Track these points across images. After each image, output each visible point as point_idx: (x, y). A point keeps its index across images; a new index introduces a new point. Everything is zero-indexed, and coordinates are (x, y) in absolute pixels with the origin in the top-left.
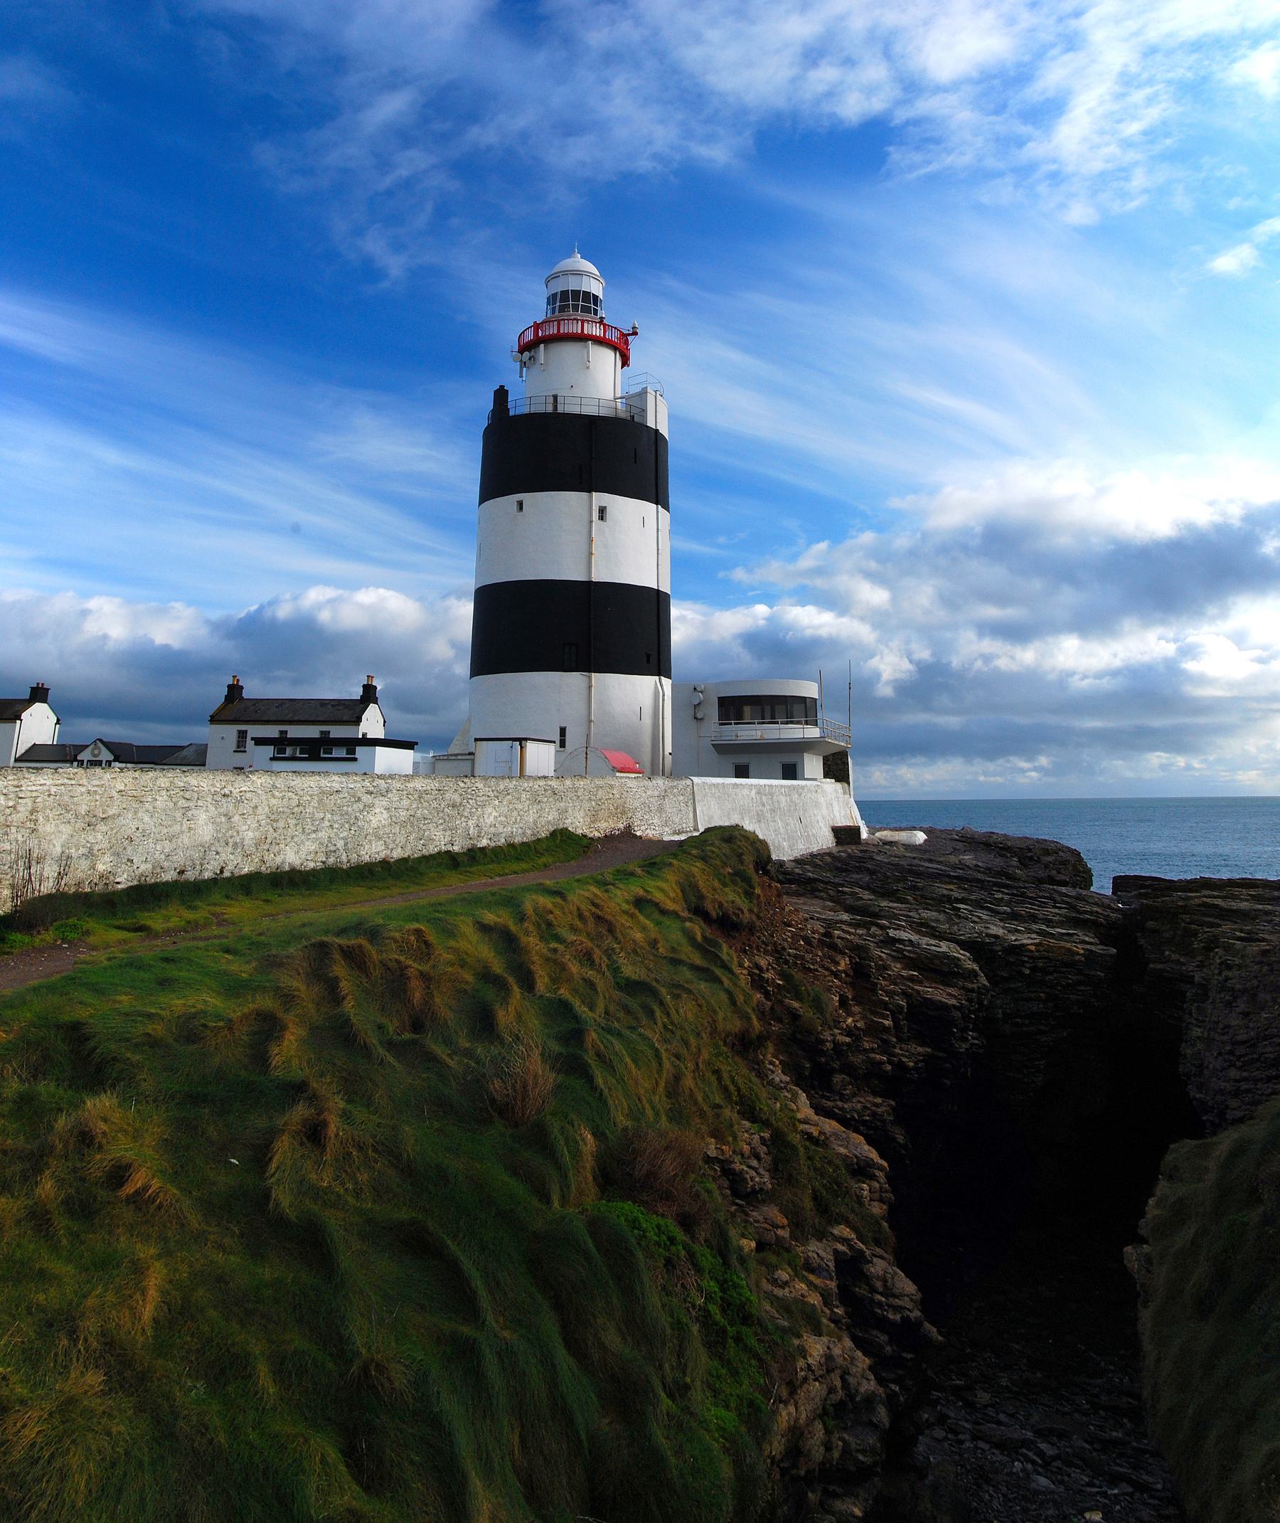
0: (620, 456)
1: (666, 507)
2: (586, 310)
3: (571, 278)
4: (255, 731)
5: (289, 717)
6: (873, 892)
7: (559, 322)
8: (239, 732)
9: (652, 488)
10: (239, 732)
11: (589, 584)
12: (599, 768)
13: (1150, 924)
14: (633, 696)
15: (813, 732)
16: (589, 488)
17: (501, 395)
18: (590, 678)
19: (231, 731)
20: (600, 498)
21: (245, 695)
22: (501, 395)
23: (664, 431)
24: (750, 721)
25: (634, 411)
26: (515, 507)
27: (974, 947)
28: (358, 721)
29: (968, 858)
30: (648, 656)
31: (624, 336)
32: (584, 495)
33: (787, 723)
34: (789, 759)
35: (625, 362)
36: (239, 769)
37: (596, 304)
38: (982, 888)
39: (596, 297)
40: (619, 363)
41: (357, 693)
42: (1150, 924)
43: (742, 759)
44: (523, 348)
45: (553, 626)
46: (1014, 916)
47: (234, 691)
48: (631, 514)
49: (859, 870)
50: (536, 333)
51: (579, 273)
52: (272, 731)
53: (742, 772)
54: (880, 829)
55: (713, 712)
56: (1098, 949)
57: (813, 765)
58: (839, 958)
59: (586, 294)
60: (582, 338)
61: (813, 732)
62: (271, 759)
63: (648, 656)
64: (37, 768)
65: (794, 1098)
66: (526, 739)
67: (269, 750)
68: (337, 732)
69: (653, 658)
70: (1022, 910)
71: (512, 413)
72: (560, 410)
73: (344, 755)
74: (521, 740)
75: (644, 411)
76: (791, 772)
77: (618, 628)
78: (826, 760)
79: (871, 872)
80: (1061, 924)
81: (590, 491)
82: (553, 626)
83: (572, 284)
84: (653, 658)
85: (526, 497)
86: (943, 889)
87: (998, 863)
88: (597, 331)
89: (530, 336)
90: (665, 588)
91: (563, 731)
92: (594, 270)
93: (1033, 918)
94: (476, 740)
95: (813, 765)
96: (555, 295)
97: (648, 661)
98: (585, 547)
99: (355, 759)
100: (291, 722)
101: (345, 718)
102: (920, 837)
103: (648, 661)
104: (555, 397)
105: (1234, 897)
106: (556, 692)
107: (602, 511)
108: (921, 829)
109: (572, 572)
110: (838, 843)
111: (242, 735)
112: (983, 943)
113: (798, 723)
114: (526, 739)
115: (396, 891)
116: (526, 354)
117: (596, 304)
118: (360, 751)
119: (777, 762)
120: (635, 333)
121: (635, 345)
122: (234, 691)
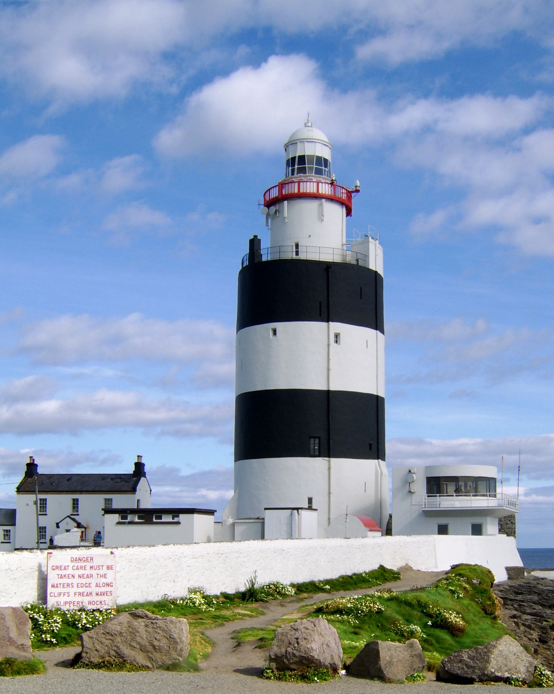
0: (345, 294)
1: (382, 332)
2: (319, 172)
5: (79, 488)
7: (299, 183)
8: (74, 500)
10: (74, 500)
14: (353, 476)
17: (254, 243)
18: (329, 461)
19: (30, 498)
20: (336, 327)
21: (40, 471)
22: (254, 243)
23: (381, 271)
25: (359, 256)
26: (271, 333)
30: (370, 445)
31: (349, 193)
32: (325, 324)
34: (477, 520)
35: (349, 213)
37: (326, 166)
39: (326, 161)
40: (345, 215)
41: (130, 469)
43: (443, 521)
44: (269, 204)
47: (31, 467)
48: (355, 336)
50: (280, 191)
53: (443, 530)
54: (533, 570)
59: (319, 159)
60: (316, 197)
62: (119, 523)
63: (370, 445)
66: (301, 508)
67: (116, 517)
69: (374, 448)
71: (264, 259)
72: (302, 256)
73: (171, 520)
74: (297, 509)
76: (477, 530)
77: (344, 425)
78: (500, 520)
79: (539, 594)
81: (328, 321)
84: (374, 448)
85: (279, 326)
88: (325, 189)
89: (275, 193)
90: (381, 394)
91: (310, 500)
94: (266, 509)
96: (293, 159)
97: (370, 449)
99: (178, 523)
100: (81, 492)
103: (370, 449)
104: (297, 246)
106: (300, 474)
107: (337, 336)
109: (314, 382)
110: (509, 578)
113: (483, 495)
116: (273, 209)
118: (182, 517)
120: (357, 191)
121: (356, 200)
122: (31, 467)
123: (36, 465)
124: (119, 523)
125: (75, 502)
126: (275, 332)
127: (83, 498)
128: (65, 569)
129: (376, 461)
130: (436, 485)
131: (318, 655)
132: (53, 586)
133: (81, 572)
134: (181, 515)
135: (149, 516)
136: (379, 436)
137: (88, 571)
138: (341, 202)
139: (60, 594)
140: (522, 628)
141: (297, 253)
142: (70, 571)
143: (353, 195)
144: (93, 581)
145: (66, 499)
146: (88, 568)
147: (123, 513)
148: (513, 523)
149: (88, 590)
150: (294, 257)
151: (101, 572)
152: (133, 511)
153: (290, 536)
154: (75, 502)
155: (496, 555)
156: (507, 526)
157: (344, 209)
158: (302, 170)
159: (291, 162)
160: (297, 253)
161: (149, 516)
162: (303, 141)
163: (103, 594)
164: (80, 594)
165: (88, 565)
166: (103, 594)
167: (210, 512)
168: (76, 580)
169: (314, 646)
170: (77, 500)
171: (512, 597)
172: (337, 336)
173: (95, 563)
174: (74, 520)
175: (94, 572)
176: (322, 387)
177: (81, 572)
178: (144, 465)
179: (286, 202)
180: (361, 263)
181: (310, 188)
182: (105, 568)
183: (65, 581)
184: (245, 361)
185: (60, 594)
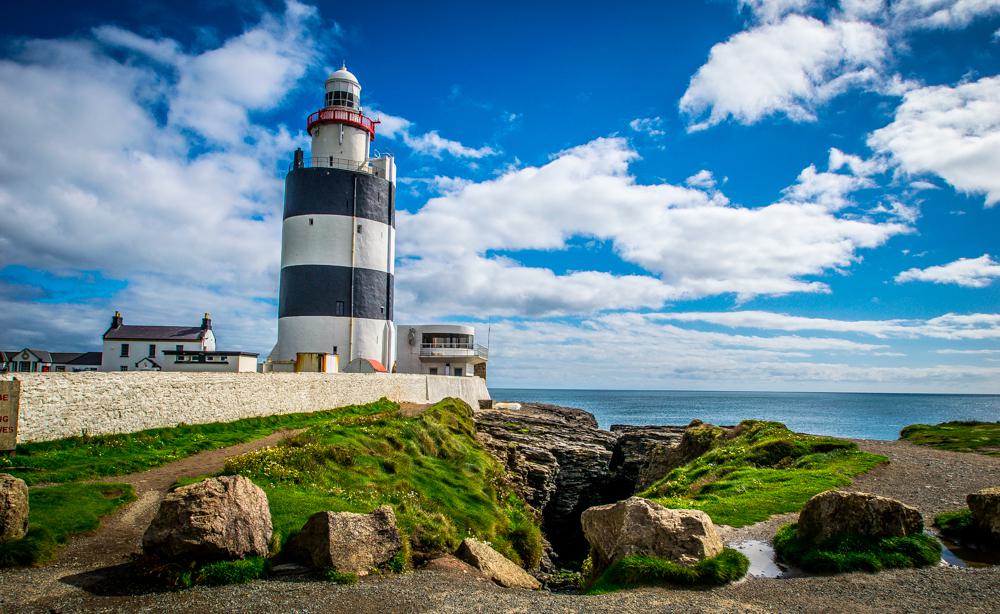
3: (342, 84)
4: (161, 346)
12: (361, 373)
13: (628, 442)
15: (471, 353)
19: (118, 345)
21: (124, 323)
24: (433, 348)
27: (554, 451)
28: (200, 339)
34: (458, 366)
36: (124, 368)
41: (199, 324)
42: (628, 442)
43: (434, 366)
45: (317, 291)
46: (571, 439)
49: (498, 419)
51: (347, 82)
52: (172, 346)
53: (433, 371)
55: (419, 338)
56: (605, 452)
57: (469, 369)
60: (348, 123)
61: (471, 353)
62: (176, 362)
64: (92, 369)
65: (641, 515)
67: (174, 358)
68: (188, 347)
70: (574, 436)
76: (459, 372)
80: (590, 442)
82: (317, 291)
83: (342, 88)
86: (539, 428)
89: (316, 118)
92: (355, 80)
93: (579, 440)
95: (469, 369)
96: (331, 93)
100: (157, 340)
104: (331, 158)
105: (664, 431)
107: (359, 227)
111: (153, 348)
114: (238, 354)
115: (832, 420)
118: (229, 359)
122: (116, 321)
124: (176, 362)
126: (312, 222)
130: (428, 339)
131: (224, 542)
135: (202, 357)
136: (390, 309)
141: (331, 165)
143: (376, 125)
145: (146, 345)
148: (484, 369)
153: (320, 371)
155: (472, 391)
156: (480, 370)
158: (337, 103)
159: (329, 96)
160: (331, 165)
161: (202, 357)
167: (255, 356)
169: (219, 524)
171: (485, 422)
172: (359, 227)
174: (151, 361)
184: (289, 243)
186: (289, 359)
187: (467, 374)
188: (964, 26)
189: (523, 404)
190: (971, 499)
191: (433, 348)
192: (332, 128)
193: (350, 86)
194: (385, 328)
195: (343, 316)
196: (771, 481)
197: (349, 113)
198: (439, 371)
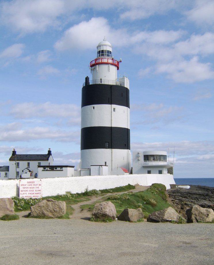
0: (117, 95)
1: (129, 108)
2: (108, 55)
6: (182, 197)
8: (28, 163)
9: (126, 103)
10: (28, 163)
11: (111, 127)
14: (120, 155)
16: (111, 103)
17: (87, 79)
18: (112, 150)
20: (114, 106)
21: (17, 153)
22: (87, 79)
23: (128, 88)
24: (150, 161)
25: (121, 83)
26: (93, 108)
28: (48, 160)
29: (200, 192)
31: (118, 63)
33: (160, 161)
34: (160, 169)
35: (118, 69)
37: (110, 54)
38: (203, 196)
39: (110, 52)
41: (47, 153)
43: (149, 169)
45: (94, 138)
47: (14, 153)
48: (120, 109)
50: (95, 62)
53: (149, 172)
55: (142, 158)
57: (165, 171)
58: (178, 205)
60: (107, 64)
62: (43, 170)
66: (103, 165)
67: (42, 169)
69: (126, 145)
71: (90, 84)
73: (60, 169)
75: (124, 83)
76: (160, 172)
77: (118, 138)
78: (168, 169)
82: (94, 138)
85: (95, 106)
86: (195, 196)
87: (206, 193)
88: (110, 61)
89: (94, 62)
91: (106, 163)
94: (91, 166)
95: (165, 171)
96: (100, 51)
98: (111, 118)
99: (62, 170)
100: (30, 160)
101: (45, 159)
102: (188, 187)
103: (125, 146)
104: (101, 80)
107: (114, 109)
108: (188, 185)
110: (171, 188)
112: (203, 205)
116: (93, 68)
117: (110, 54)
118: (64, 168)
119: (157, 170)
120: (121, 62)
121: (120, 65)
122: (14, 153)
123: (16, 152)
124: (43, 170)
125: (29, 164)
126: (94, 108)
127: (31, 162)
128: (25, 185)
129: (127, 150)
130: (147, 158)
132: (21, 191)
133: (31, 186)
134: (63, 168)
135: (53, 168)
137: (33, 186)
138: (116, 66)
139: (23, 194)
140: (175, 204)
141: (101, 82)
142: (27, 186)
144: (34, 189)
145: (26, 163)
146: (33, 185)
147: (44, 167)
149: (33, 192)
150: (100, 83)
151: (37, 186)
152: (47, 167)
153: (99, 174)
154: (29, 164)
155: (166, 180)
156: (170, 171)
157: (116, 68)
158: (103, 55)
160: (101, 82)
161: (53, 168)
162: (103, 45)
163: (38, 193)
164: (30, 194)
165: (33, 184)
166: (38, 193)
167: (73, 167)
168: (29, 189)
170: (29, 163)
172: (114, 109)
173: (35, 184)
174: (28, 169)
175: (35, 186)
176: (108, 125)
177: (31, 186)
178: (51, 151)
179: (97, 65)
180: (122, 85)
181: (105, 61)
182: (38, 185)
183: (25, 189)
185: (23, 194)
186: (86, 169)
187: (164, 173)
188: (93, 18)
189: (190, 186)
190: (69, 218)
191: (150, 161)
192: (106, 66)
193: (102, 47)
194: (127, 153)
195: (108, 148)
196: (196, 219)
197: (108, 59)
198: (152, 172)
